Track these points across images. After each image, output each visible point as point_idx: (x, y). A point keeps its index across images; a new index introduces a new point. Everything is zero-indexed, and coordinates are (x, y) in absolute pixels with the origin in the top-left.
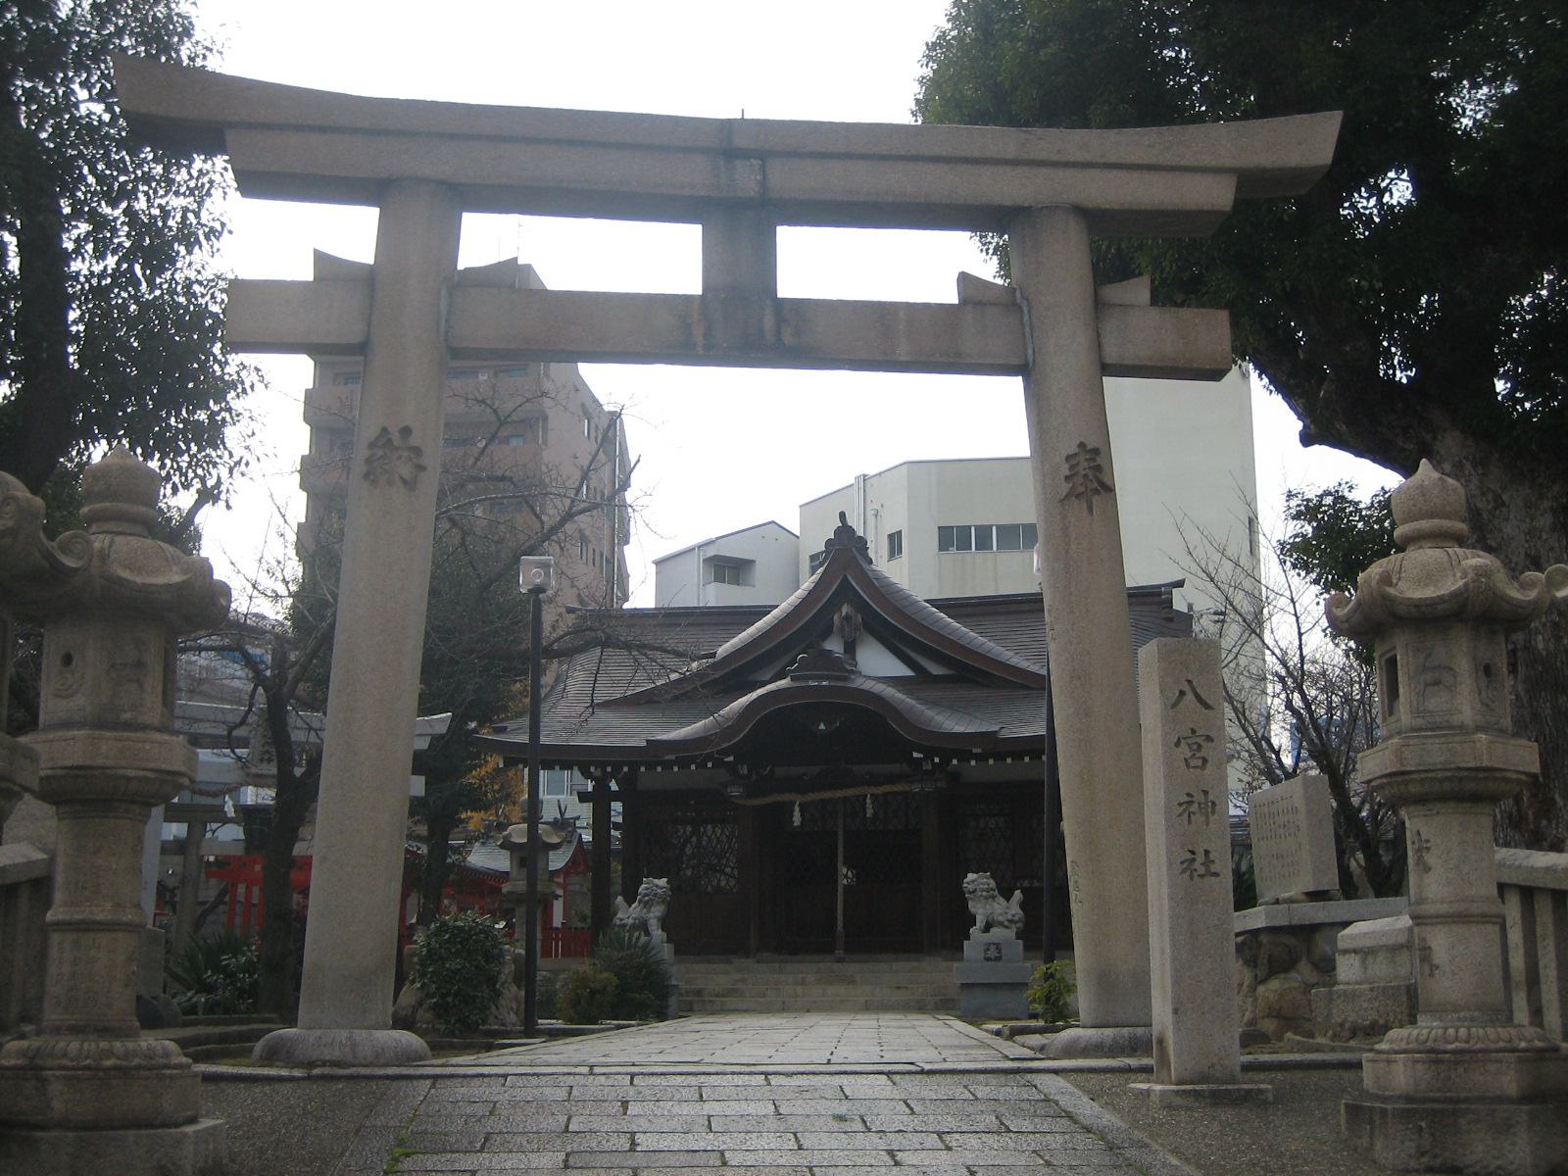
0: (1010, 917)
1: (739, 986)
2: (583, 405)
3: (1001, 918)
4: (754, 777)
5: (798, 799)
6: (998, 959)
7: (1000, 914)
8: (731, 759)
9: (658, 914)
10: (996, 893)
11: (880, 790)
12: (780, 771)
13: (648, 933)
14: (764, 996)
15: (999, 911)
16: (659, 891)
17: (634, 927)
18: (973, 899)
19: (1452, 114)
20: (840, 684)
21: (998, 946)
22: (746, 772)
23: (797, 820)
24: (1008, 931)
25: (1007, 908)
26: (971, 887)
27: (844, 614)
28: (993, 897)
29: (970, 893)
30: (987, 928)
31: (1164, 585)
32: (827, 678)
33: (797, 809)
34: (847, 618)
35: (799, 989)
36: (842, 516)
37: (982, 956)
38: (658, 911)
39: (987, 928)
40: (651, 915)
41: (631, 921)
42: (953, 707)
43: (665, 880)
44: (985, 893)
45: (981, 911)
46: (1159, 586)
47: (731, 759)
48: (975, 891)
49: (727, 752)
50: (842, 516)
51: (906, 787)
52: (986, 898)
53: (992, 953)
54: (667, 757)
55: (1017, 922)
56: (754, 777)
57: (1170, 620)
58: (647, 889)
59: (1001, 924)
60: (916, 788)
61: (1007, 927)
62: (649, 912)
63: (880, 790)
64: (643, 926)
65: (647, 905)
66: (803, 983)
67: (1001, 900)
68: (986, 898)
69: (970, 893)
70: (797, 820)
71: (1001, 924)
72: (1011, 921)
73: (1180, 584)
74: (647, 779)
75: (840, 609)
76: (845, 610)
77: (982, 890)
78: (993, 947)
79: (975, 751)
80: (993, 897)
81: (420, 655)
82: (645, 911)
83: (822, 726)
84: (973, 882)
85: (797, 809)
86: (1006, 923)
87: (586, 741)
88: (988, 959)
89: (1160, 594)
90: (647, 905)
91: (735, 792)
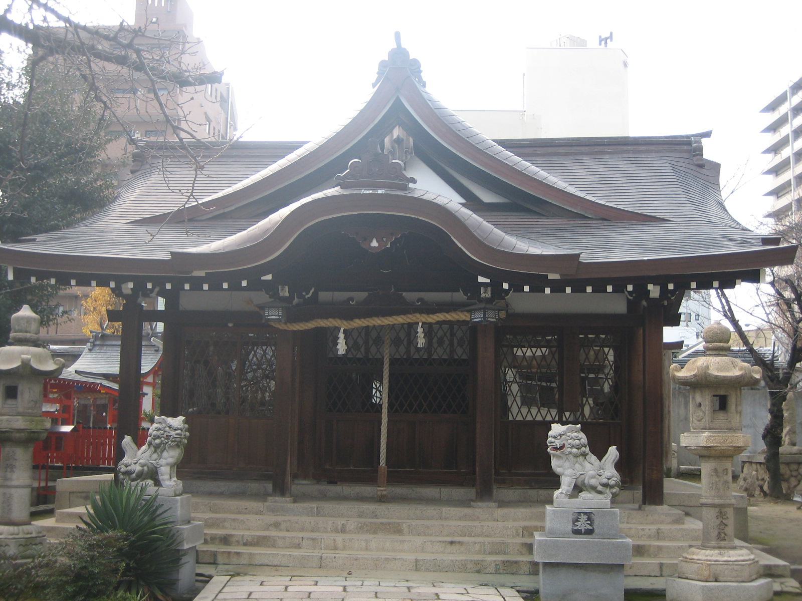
0: (605, 481)
1: (273, 533)
2: (206, 113)
3: (593, 482)
4: (296, 301)
5: (344, 325)
6: (590, 532)
7: (593, 477)
8: (269, 277)
9: (171, 460)
10: (587, 450)
11: (433, 318)
12: (324, 296)
13: (157, 483)
14: (299, 546)
15: (592, 473)
16: (173, 433)
17: (141, 476)
18: (559, 457)
19: (185, 422)
20: (398, 193)
21: (589, 517)
22: (287, 294)
23: (342, 348)
24: (601, 496)
25: (601, 468)
26: (558, 442)
27: (395, 136)
28: (584, 455)
29: (556, 449)
30: (578, 489)
31: (693, 136)
32: (381, 187)
33: (341, 336)
34: (399, 141)
35: (340, 538)
36: (397, 36)
37: (570, 527)
38: (171, 456)
39: (578, 489)
40: (162, 461)
41: (138, 468)
42: (524, 233)
43: (181, 418)
44: (574, 450)
45: (569, 472)
46: (688, 137)
47: (269, 277)
48: (562, 447)
49: (264, 269)
50: (397, 36)
51: (463, 316)
52: (576, 456)
53: (582, 525)
54: (197, 273)
55: (612, 487)
56: (296, 301)
57: (701, 166)
58: (158, 429)
59: (594, 488)
60: (477, 317)
61: (600, 493)
62: (160, 457)
63: (433, 318)
64: (153, 474)
65: (158, 449)
66: (343, 530)
67: (593, 458)
68: (576, 456)
69: (556, 449)
70: (342, 348)
71: (594, 488)
72: (606, 485)
73: (708, 135)
74: (190, 301)
75: (391, 132)
76: (397, 132)
77: (572, 447)
78: (583, 518)
79: (551, 276)
80: (584, 455)
81: (740, 541)
82: (155, 456)
83: (375, 244)
84: (561, 435)
85: (341, 336)
86: (600, 488)
87: (107, 253)
88: (577, 532)
89: (689, 143)
90: (158, 449)
91: (273, 315)
